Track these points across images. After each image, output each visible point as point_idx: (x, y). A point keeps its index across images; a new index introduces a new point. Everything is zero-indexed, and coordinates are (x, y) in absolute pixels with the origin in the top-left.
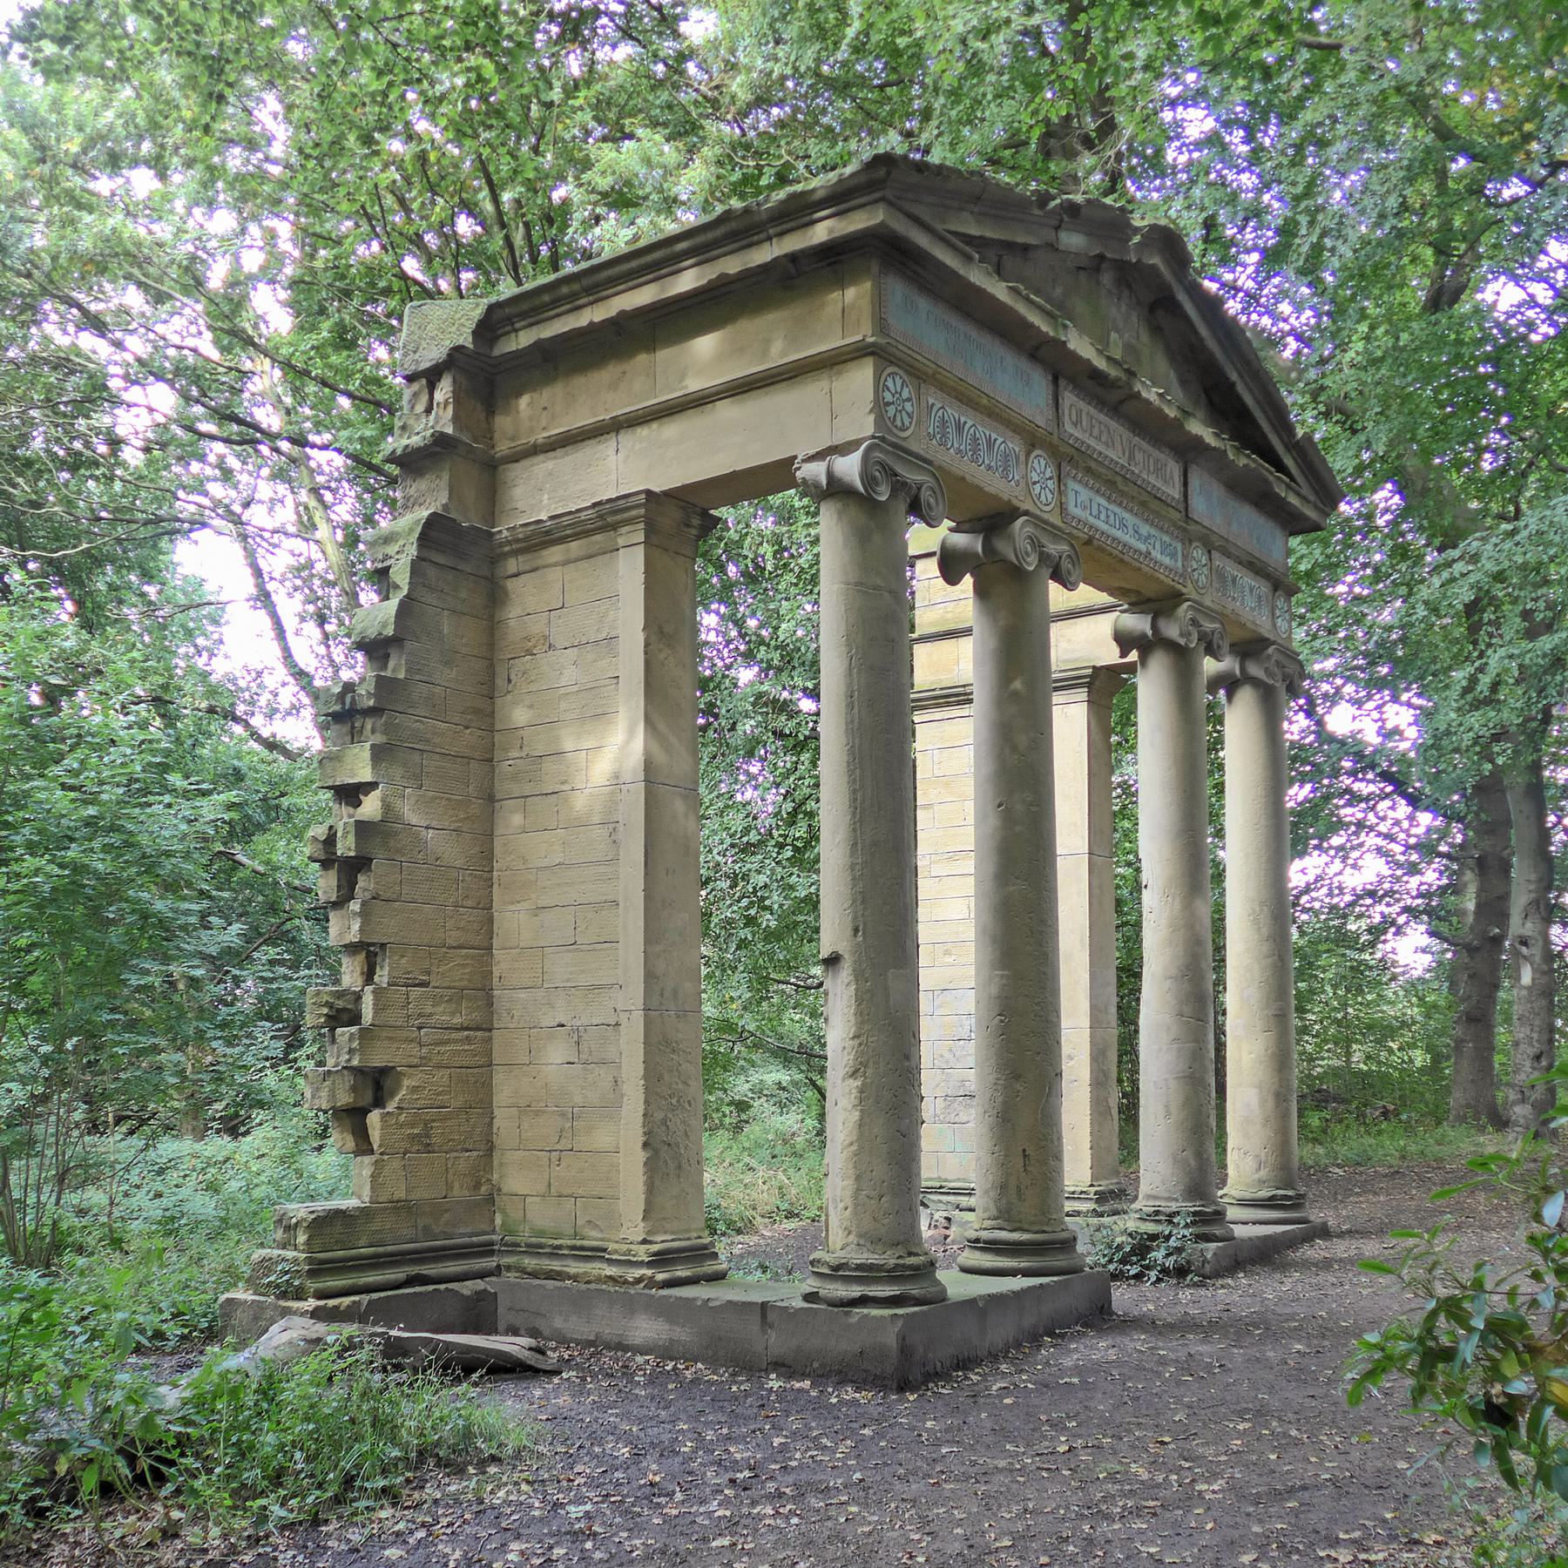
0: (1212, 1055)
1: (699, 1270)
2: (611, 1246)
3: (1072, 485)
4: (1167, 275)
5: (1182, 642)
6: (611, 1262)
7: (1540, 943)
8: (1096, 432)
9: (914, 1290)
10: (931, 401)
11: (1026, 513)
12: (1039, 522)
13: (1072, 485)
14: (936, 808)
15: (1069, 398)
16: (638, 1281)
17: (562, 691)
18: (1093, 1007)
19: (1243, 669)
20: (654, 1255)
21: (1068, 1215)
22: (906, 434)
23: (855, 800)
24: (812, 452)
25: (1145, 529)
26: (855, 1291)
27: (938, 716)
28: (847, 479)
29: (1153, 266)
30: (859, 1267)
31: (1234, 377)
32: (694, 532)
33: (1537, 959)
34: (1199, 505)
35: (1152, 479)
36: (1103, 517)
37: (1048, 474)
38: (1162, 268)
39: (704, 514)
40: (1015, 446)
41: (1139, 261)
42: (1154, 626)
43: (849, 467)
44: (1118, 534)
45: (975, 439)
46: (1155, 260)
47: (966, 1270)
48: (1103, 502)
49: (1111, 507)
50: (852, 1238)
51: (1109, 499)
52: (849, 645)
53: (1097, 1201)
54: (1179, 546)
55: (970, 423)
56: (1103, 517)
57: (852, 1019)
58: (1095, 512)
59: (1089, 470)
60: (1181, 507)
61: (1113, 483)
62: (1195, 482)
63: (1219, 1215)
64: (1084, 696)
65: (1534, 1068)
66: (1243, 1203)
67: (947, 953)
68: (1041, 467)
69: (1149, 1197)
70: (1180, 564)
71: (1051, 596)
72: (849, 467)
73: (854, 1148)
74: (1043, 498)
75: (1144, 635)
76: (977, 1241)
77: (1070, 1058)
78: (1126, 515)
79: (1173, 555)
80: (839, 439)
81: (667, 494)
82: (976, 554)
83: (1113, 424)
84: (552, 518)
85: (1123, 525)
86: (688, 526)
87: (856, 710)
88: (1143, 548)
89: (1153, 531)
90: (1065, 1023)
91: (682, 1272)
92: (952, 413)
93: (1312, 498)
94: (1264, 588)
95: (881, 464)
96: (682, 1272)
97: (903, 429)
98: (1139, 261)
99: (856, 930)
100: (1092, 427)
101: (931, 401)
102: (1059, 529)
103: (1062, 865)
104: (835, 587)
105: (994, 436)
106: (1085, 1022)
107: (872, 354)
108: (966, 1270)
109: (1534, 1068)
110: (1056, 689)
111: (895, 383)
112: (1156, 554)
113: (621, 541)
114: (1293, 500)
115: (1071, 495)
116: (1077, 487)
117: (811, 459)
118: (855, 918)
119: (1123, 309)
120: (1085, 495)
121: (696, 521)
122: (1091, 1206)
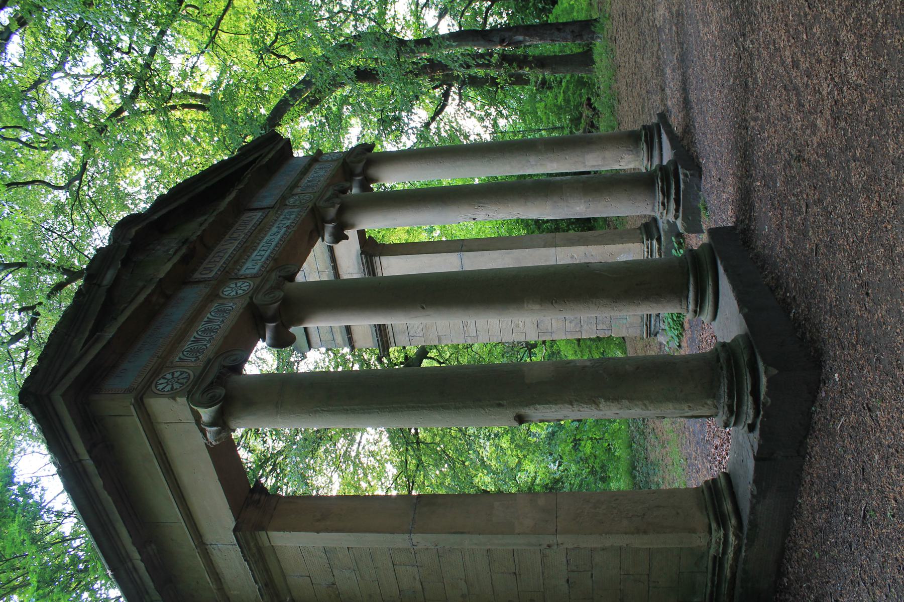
0: (569, 177)
1: (726, 493)
2: (712, 552)
3: (242, 272)
4: (144, 223)
5: (338, 206)
6: (725, 552)
7: (502, 33)
8: (218, 259)
9: (744, 359)
10: (177, 359)
11: (251, 298)
12: (257, 290)
13: (242, 272)
14: (440, 334)
15: (197, 276)
16: (737, 537)
17: (359, 578)
18: (545, 246)
19: (358, 175)
20: (718, 525)
21: (661, 256)
22: (191, 373)
23: (413, 407)
24: (201, 435)
25: (274, 229)
26: (748, 401)
27: (391, 334)
28: (213, 414)
29: (137, 233)
30: (731, 397)
31: (203, 187)
32: (263, 497)
33: (510, 34)
34: (268, 202)
35: (249, 227)
36: (263, 253)
37: (233, 286)
38: (137, 228)
39: (252, 491)
40: (214, 306)
41: (131, 240)
42: (330, 222)
43: (206, 414)
44: (274, 244)
45: (205, 331)
46: (133, 232)
47: (715, 317)
48: (255, 253)
49: (259, 248)
50: (709, 402)
51: (254, 250)
52: (316, 412)
53: (652, 240)
54: (286, 211)
55: (195, 334)
56: (263, 253)
57: (559, 406)
58: (259, 258)
59: (236, 262)
60: (267, 210)
61: (246, 249)
62: (256, 205)
63: (661, 168)
64: (377, 259)
65: (564, 31)
66: (650, 157)
67: (517, 326)
68: (229, 291)
69: (653, 210)
70: (296, 210)
71: (313, 277)
72: (206, 414)
73: (647, 402)
74: (246, 288)
75: (335, 227)
76: (695, 312)
77: (572, 257)
78: (265, 240)
79: (291, 213)
80: (191, 418)
81: (237, 516)
82: (276, 327)
83: (216, 250)
84: (256, 582)
85: (270, 241)
86: (259, 501)
87: (356, 407)
88: (283, 230)
89: (276, 225)
90: (552, 262)
91: (728, 506)
92: (187, 346)
93: (271, 146)
94: (317, 166)
95: (203, 393)
96: (728, 506)
97: (188, 378)
98: (131, 240)
99: (500, 405)
100: (215, 261)
101: (177, 359)
102: (263, 279)
103: (468, 267)
104: (279, 420)
105: (206, 319)
106: (552, 250)
107: (142, 399)
108: (715, 317)
109: (564, 31)
110: (374, 274)
111: (162, 384)
112: (288, 223)
113: (267, 544)
114: (270, 156)
115: (248, 272)
116: (244, 268)
117: (205, 435)
118: (491, 406)
119: (159, 247)
120: (249, 264)
121: (256, 497)
122: (655, 242)
